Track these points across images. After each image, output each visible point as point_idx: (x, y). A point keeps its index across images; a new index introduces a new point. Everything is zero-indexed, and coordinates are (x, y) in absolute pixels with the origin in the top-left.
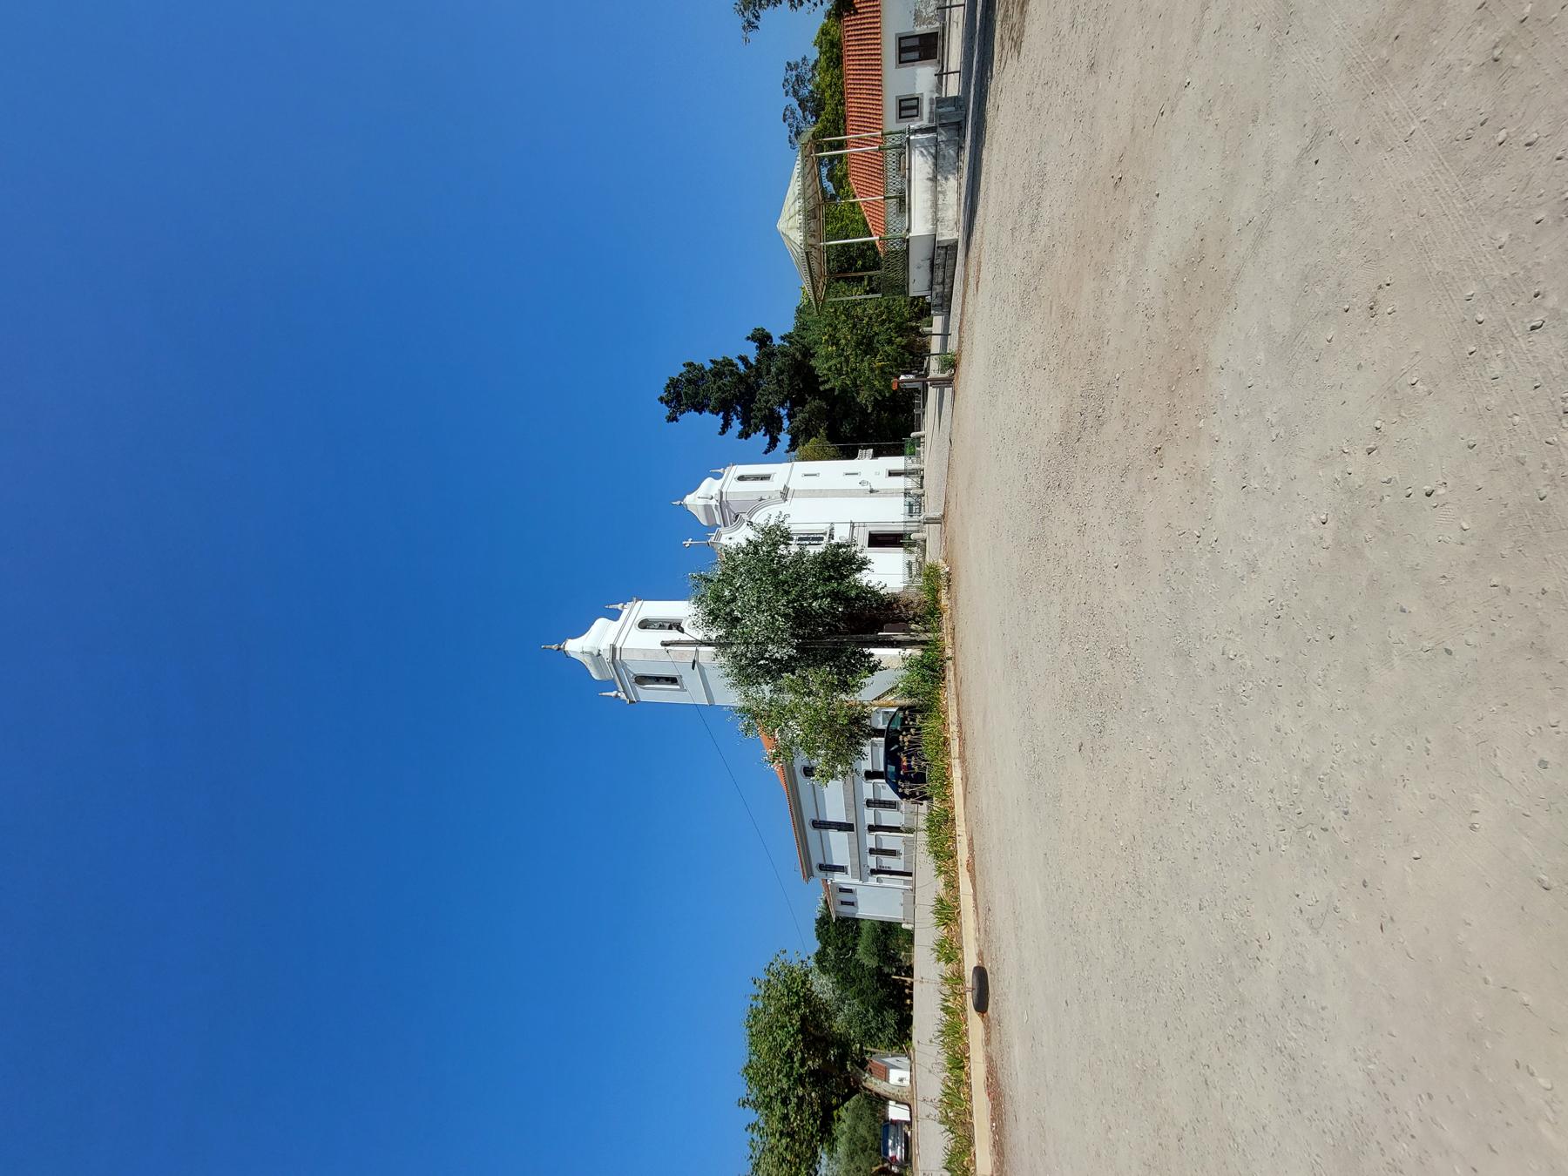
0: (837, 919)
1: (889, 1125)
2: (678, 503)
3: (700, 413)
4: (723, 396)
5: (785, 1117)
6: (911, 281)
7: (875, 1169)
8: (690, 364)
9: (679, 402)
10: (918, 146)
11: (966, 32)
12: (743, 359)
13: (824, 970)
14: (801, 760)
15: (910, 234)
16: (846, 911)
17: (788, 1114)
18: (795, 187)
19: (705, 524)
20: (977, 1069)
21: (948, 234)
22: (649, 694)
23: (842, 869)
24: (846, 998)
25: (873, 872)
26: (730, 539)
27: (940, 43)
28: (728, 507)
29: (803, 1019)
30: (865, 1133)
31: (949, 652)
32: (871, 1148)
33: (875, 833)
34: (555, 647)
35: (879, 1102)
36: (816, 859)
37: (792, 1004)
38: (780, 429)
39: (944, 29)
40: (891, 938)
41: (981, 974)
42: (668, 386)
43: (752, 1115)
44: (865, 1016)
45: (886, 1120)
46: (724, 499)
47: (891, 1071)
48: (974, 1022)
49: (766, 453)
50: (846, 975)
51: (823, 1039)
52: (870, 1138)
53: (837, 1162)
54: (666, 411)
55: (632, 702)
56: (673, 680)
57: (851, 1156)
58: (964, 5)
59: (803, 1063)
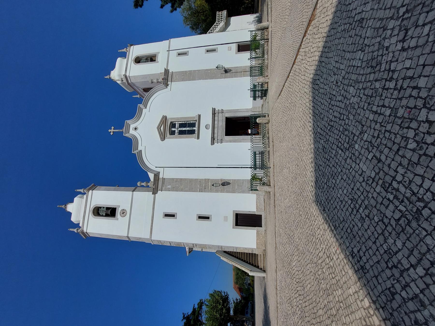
34: (63, 206)
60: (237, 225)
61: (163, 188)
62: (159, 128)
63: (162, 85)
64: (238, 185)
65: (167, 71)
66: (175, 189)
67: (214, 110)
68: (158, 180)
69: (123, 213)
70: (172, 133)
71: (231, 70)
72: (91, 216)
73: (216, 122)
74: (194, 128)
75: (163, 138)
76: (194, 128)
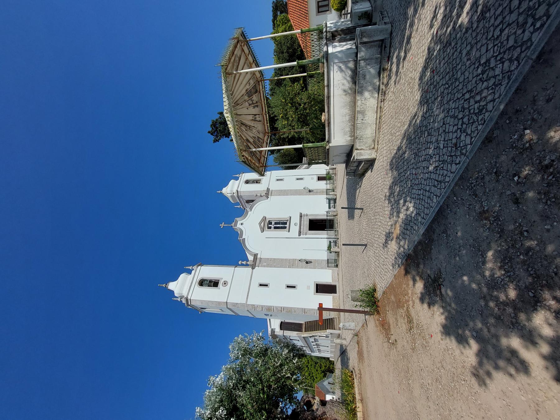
10: (336, 61)
15: (330, 145)
34: (164, 285)
54: (212, 138)
60: (317, 292)
61: (260, 265)
62: (260, 224)
63: (265, 197)
64: (318, 263)
65: (268, 190)
66: (269, 266)
67: (301, 214)
68: (256, 259)
69: (225, 284)
70: (270, 228)
71: (313, 191)
72: (197, 285)
73: (302, 222)
74: (286, 226)
75: (263, 231)
76: (286, 226)
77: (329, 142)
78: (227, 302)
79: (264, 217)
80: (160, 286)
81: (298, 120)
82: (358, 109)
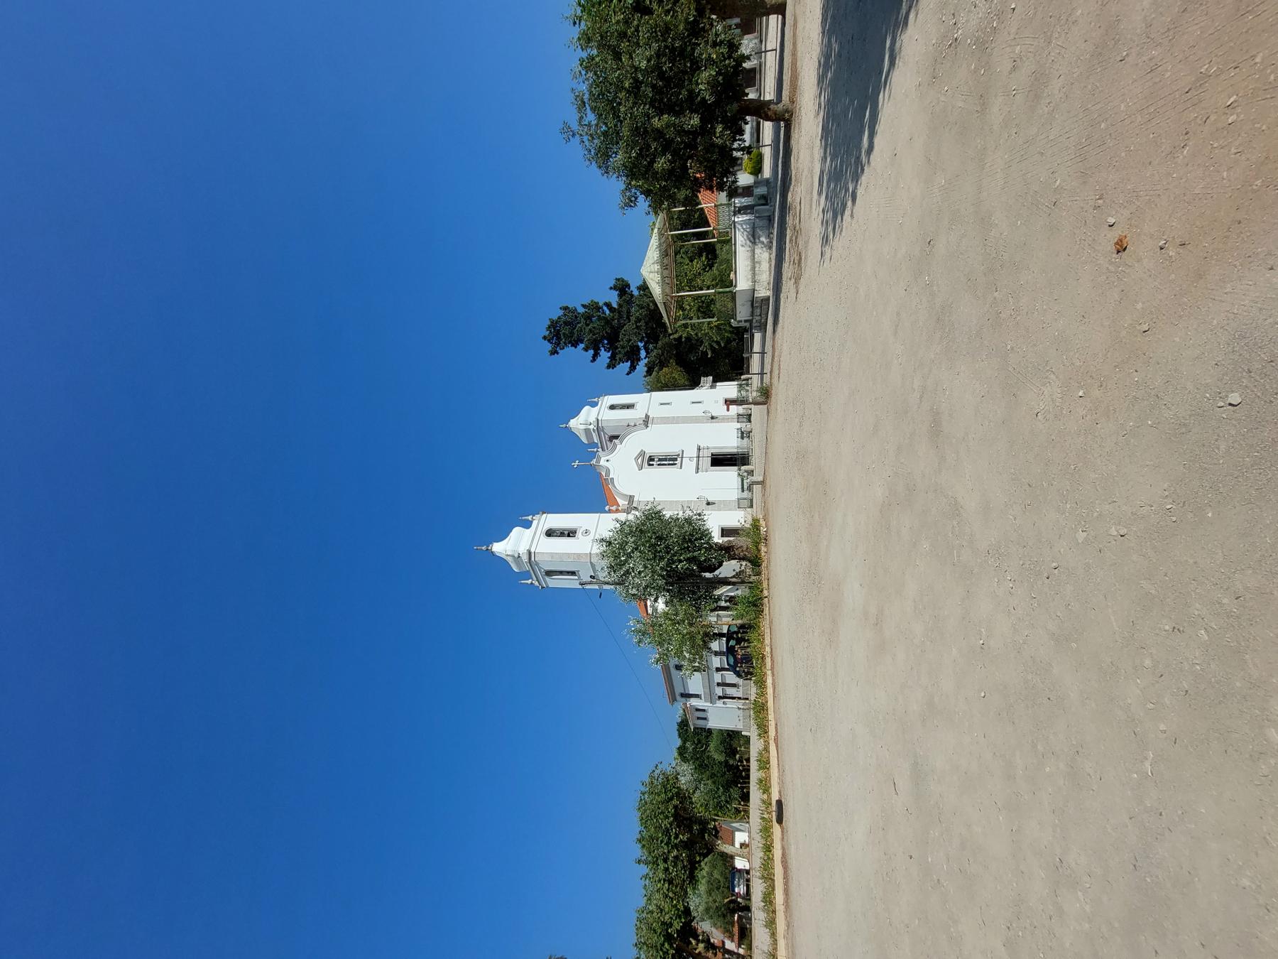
0: (695, 729)
1: (735, 871)
2: (564, 426)
3: (576, 347)
4: (594, 337)
5: (666, 869)
6: (738, 312)
7: (726, 901)
8: (566, 308)
9: (559, 338)
11: (774, 151)
12: (608, 305)
13: (684, 759)
14: (674, 661)
16: (701, 723)
17: (668, 867)
18: (654, 241)
19: (586, 442)
20: (777, 853)
21: (764, 291)
22: (555, 582)
23: (697, 696)
24: (702, 779)
25: (720, 698)
26: (608, 461)
27: (758, 76)
28: (603, 431)
29: (675, 807)
30: (719, 877)
31: (765, 593)
32: (723, 887)
33: (721, 673)
34: (484, 548)
35: (728, 859)
36: (679, 690)
37: (668, 798)
38: (639, 359)
39: (760, 66)
40: (733, 741)
41: (779, 803)
42: (549, 327)
43: (644, 869)
44: (716, 792)
45: (734, 868)
46: (600, 425)
47: (736, 833)
48: (776, 829)
49: (628, 374)
50: (702, 763)
51: (690, 819)
52: (722, 879)
53: (698, 897)
54: (549, 346)
55: (543, 587)
56: (573, 573)
57: (709, 893)
58: (776, 50)
59: (677, 837)
62: (636, 459)
65: (647, 417)
74: (676, 462)
75: (641, 468)
77: (735, 286)
78: (590, 553)
79: (642, 451)
80: (477, 549)
81: (698, 310)
82: (756, 260)
